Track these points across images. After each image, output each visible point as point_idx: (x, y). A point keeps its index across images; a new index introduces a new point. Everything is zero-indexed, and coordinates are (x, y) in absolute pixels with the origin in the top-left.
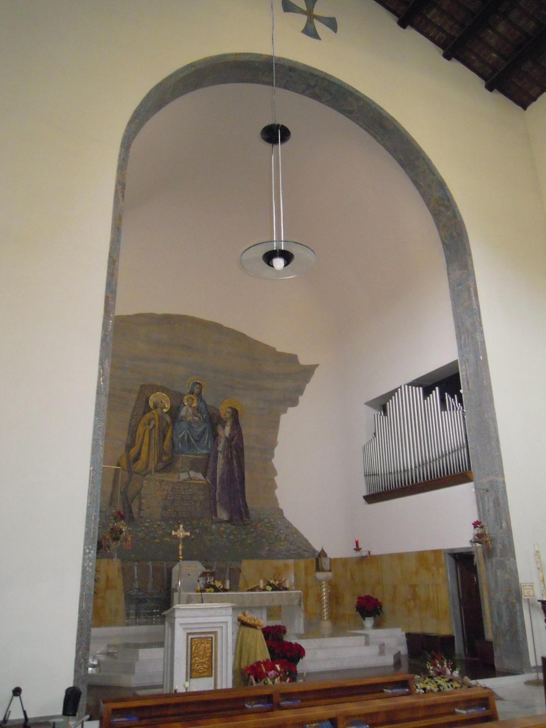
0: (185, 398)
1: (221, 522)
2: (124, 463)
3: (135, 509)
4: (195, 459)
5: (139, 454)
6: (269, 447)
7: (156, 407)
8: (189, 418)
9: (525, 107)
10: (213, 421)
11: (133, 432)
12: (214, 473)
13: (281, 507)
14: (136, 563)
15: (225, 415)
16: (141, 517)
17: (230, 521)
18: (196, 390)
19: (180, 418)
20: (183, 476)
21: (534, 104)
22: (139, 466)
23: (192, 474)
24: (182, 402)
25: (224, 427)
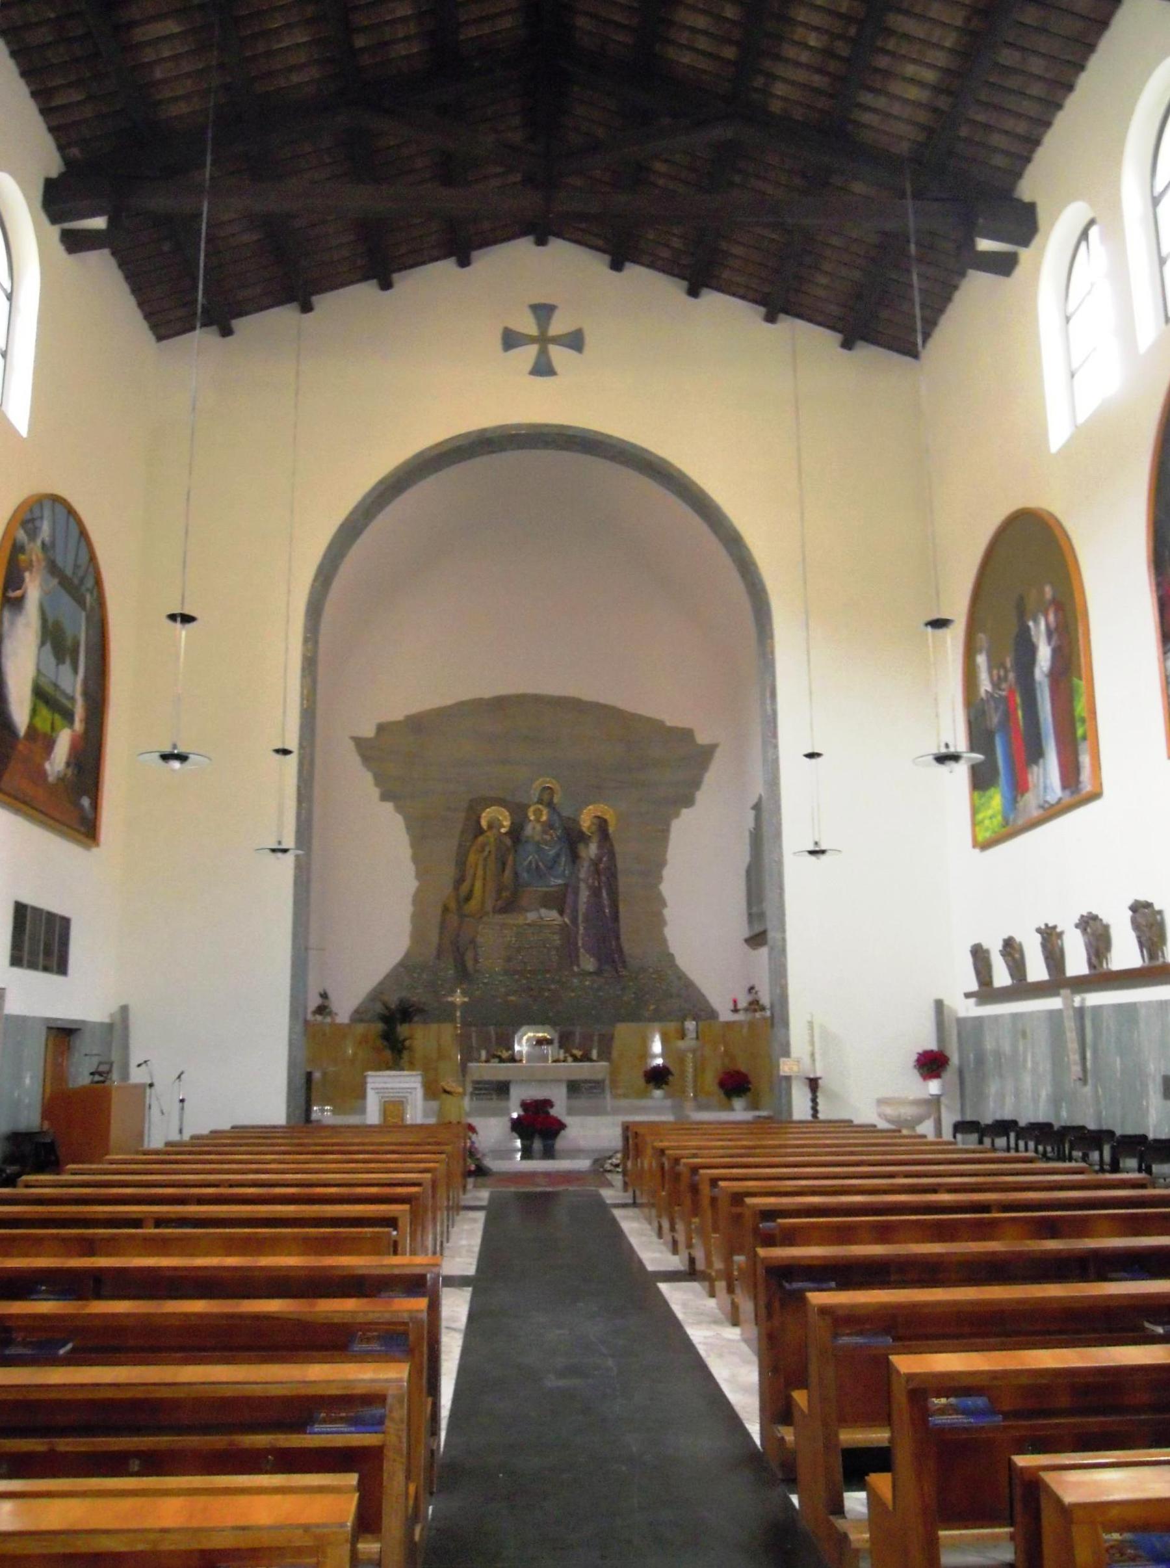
0: (532, 809)
1: (586, 974)
2: (453, 905)
3: (470, 964)
4: (546, 893)
5: (471, 892)
6: (653, 868)
7: (490, 826)
8: (537, 838)
9: (911, 351)
10: (573, 838)
11: (461, 863)
12: (575, 910)
13: (672, 950)
14: (473, 1029)
15: (589, 828)
16: (477, 971)
17: (598, 972)
18: (546, 797)
19: (524, 839)
20: (531, 916)
22: (474, 904)
23: (543, 911)
24: (526, 817)
25: (587, 845)
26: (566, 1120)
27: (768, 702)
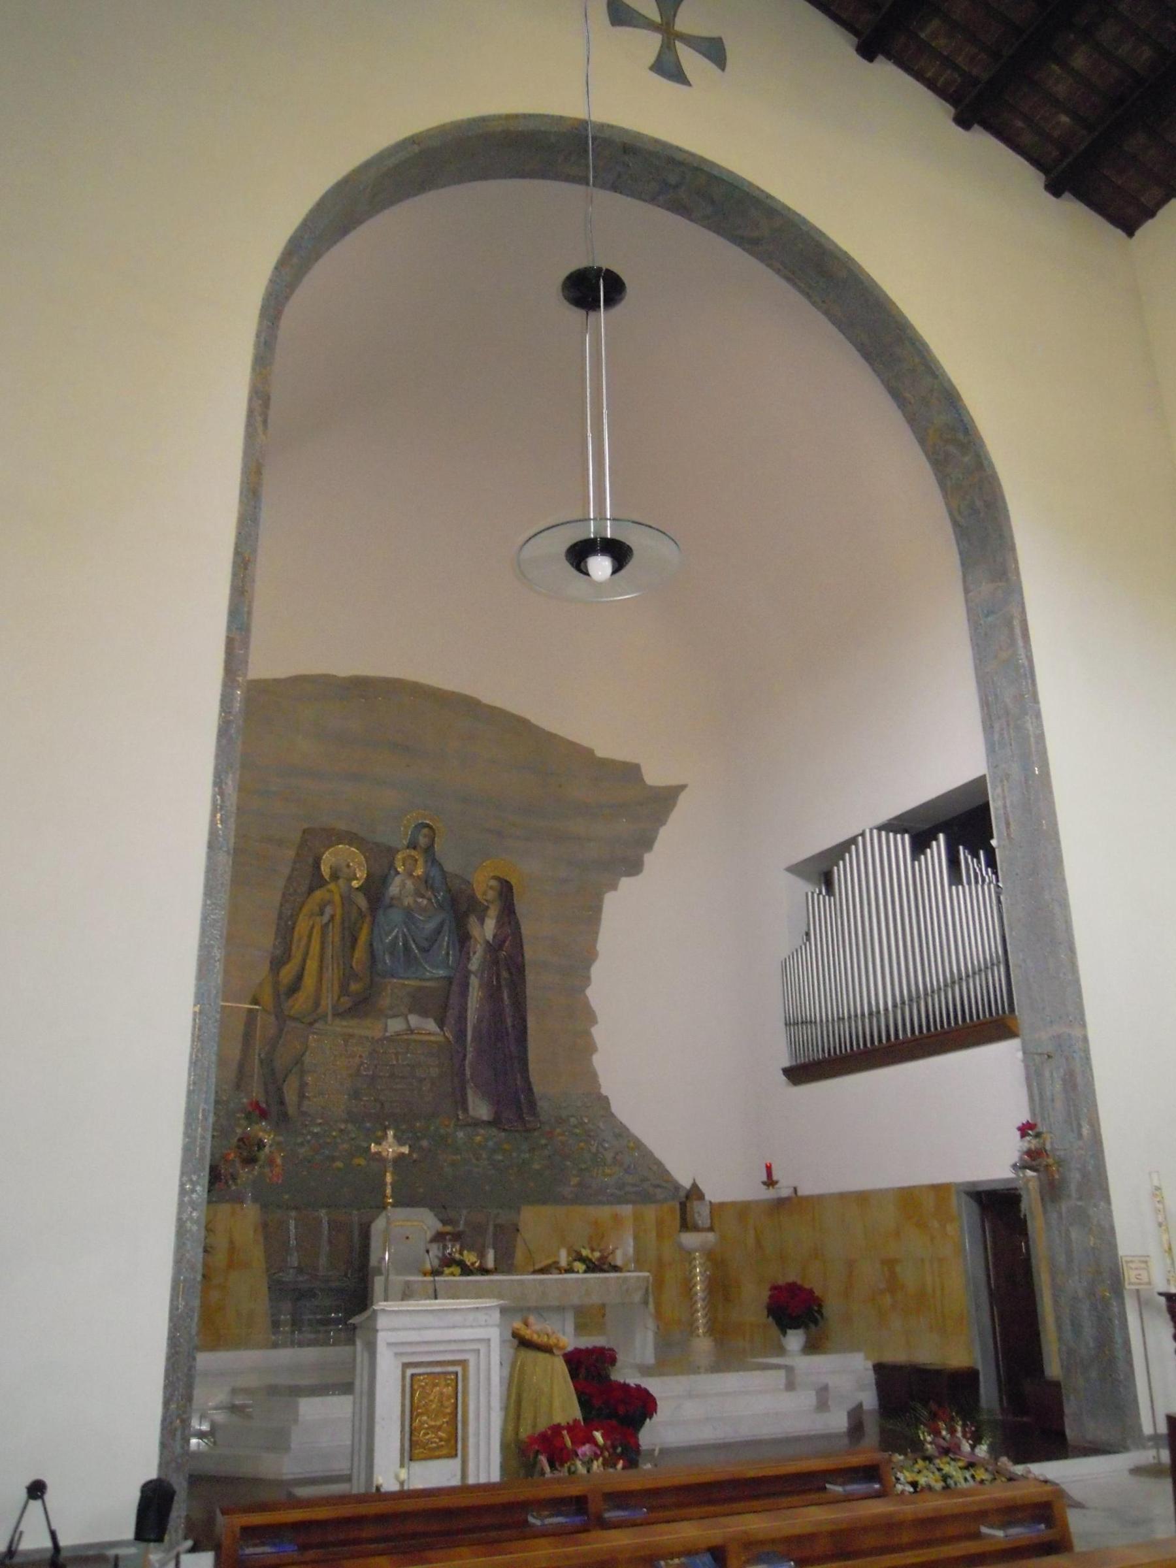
0: (399, 856)
1: (477, 1123)
2: (267, 996)
3: (291, 1097)
4: (420, 989)
5: (299, 977)
6: (578, 963)
7: (335, 876)
8: (408, 901)
10: (460, 907)
11: (286, 930)
12: (462, 1018)
13: (604, 1091)
14: (293, 1214)
15: (485, 893)
16: (304, 1114)
17: (495, 1122)
19: (387, 901)
20: (395, 1025)
21: (1150, 224)
22: (300, 1003)
23: (414, 1020)
24: (391, 866)
25: (482, 921)
26: (653, 1385)
27: (1020, 643)
